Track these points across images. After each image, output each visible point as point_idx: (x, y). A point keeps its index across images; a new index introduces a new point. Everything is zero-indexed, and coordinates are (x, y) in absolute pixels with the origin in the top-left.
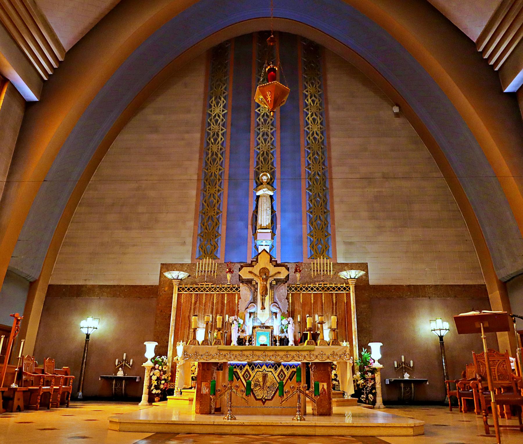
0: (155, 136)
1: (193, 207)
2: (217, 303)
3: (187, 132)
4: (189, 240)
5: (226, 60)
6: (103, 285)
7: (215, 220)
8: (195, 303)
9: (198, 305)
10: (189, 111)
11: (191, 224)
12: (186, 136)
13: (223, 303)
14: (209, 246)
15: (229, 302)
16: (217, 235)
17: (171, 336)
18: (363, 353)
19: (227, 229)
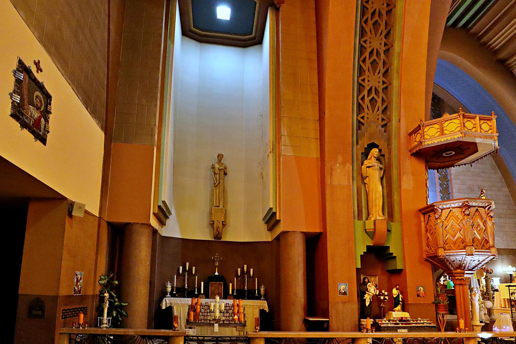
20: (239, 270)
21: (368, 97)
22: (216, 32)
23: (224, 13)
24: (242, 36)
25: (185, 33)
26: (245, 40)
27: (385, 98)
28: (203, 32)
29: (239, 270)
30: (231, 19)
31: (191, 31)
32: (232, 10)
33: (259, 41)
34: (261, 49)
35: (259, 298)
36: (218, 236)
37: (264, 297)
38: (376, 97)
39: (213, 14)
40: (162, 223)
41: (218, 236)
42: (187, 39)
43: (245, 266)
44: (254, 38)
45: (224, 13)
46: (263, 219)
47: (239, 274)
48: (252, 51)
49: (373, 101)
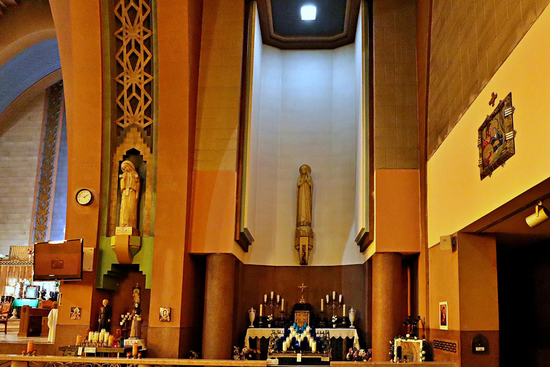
0: (7, 158)
1: (31, 209)
2: (22, 272)
3: (29, 155)
4: (28, 232)
5: (59, 97)
6: (149, 308)
7: (45, 218)
8: (9, 272)
9: (10, 273)
10: (31, 140)
11: (29, 220)
12: (28, 158)
13: (25, 272)
14: (40, 235)
15: (28, 271)
16: (45, 228)
17: (45, 359)
18: (283, 335)
19: (52, 224)
20: (266, 296)
21: (127, 53)
22: (297, 35)
23: (308, 13)
24: (329, 38)
25: (266, 41)
26: (329, 41)
27: (148, 52)
28: (287, 38)
29: (266, 296)
30: (316, 18)
31: (271, 37)
32: (318, 9)
33: (352, 40)
34: (354, 48)
35: (347, 326)
36: (304, 262)
37: (353, 325)
38: (136, 52)
39: (298, 16)
40: (245, 250)
41: (304, 262)
42: (270, 48)
43: (272, 293)
44: (346, 37)
45: (308, 13)
46: (356, 241)
47: (265, 300)
48: (341, 54)
49: (134, 58)
